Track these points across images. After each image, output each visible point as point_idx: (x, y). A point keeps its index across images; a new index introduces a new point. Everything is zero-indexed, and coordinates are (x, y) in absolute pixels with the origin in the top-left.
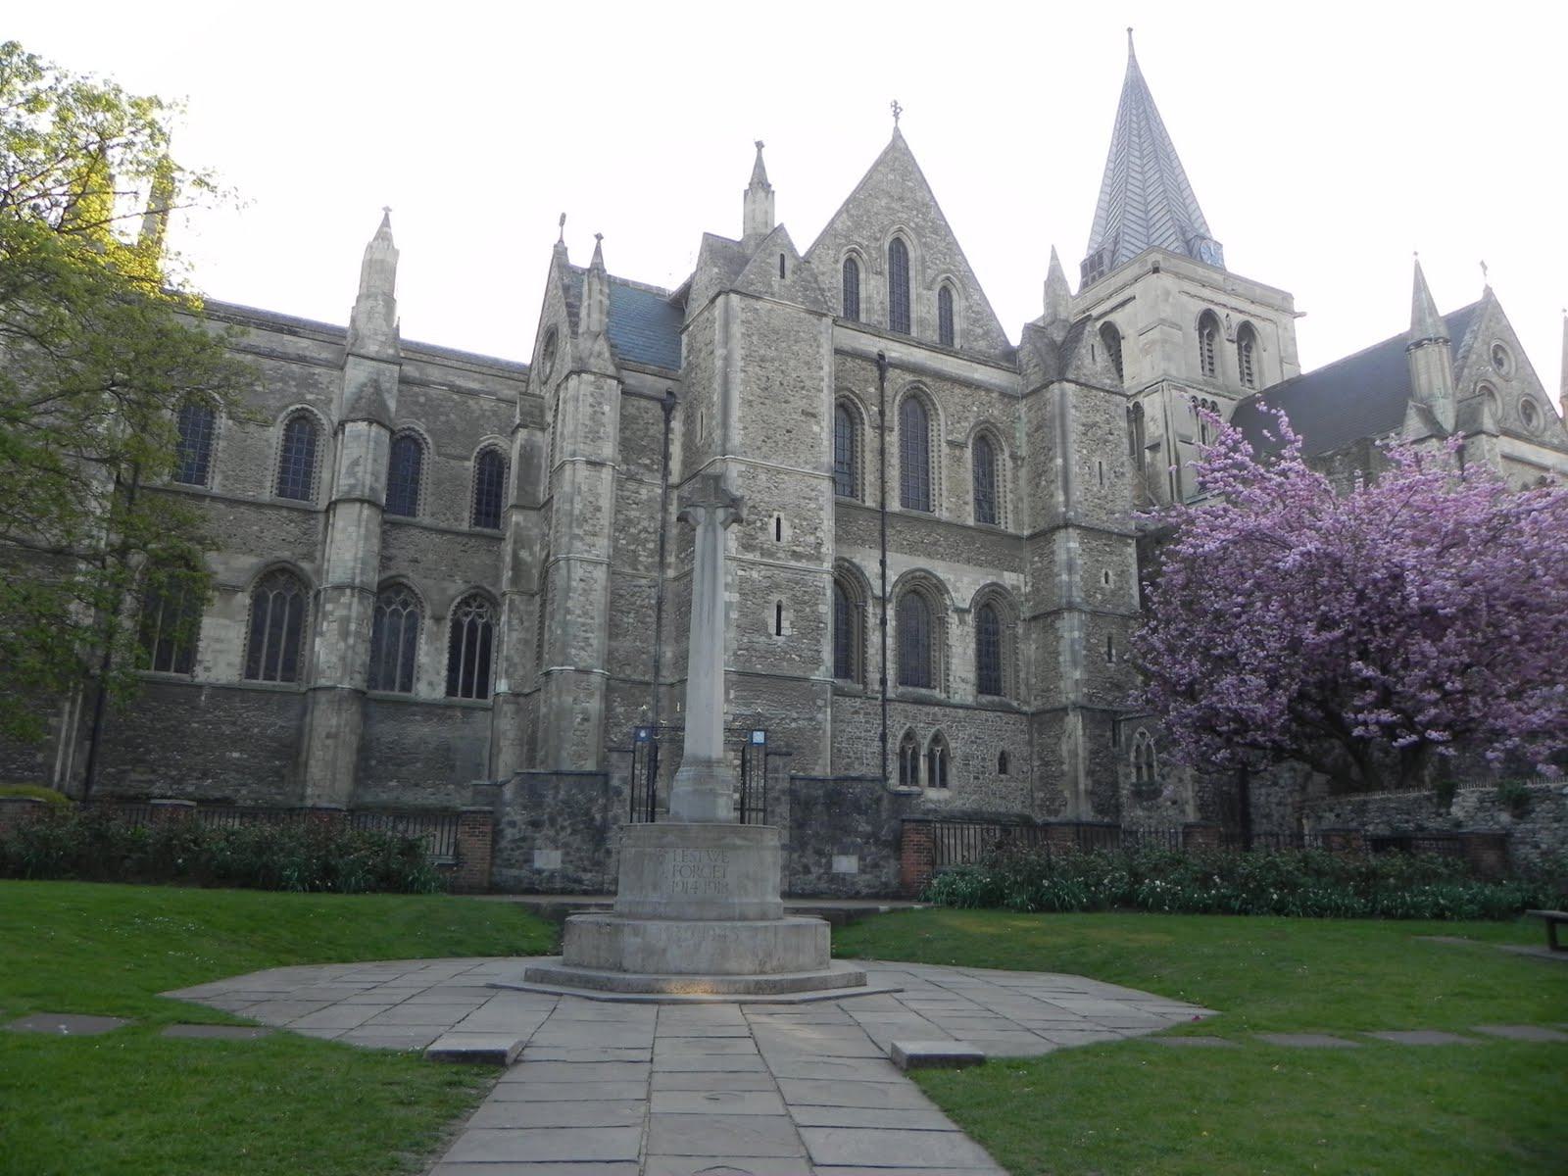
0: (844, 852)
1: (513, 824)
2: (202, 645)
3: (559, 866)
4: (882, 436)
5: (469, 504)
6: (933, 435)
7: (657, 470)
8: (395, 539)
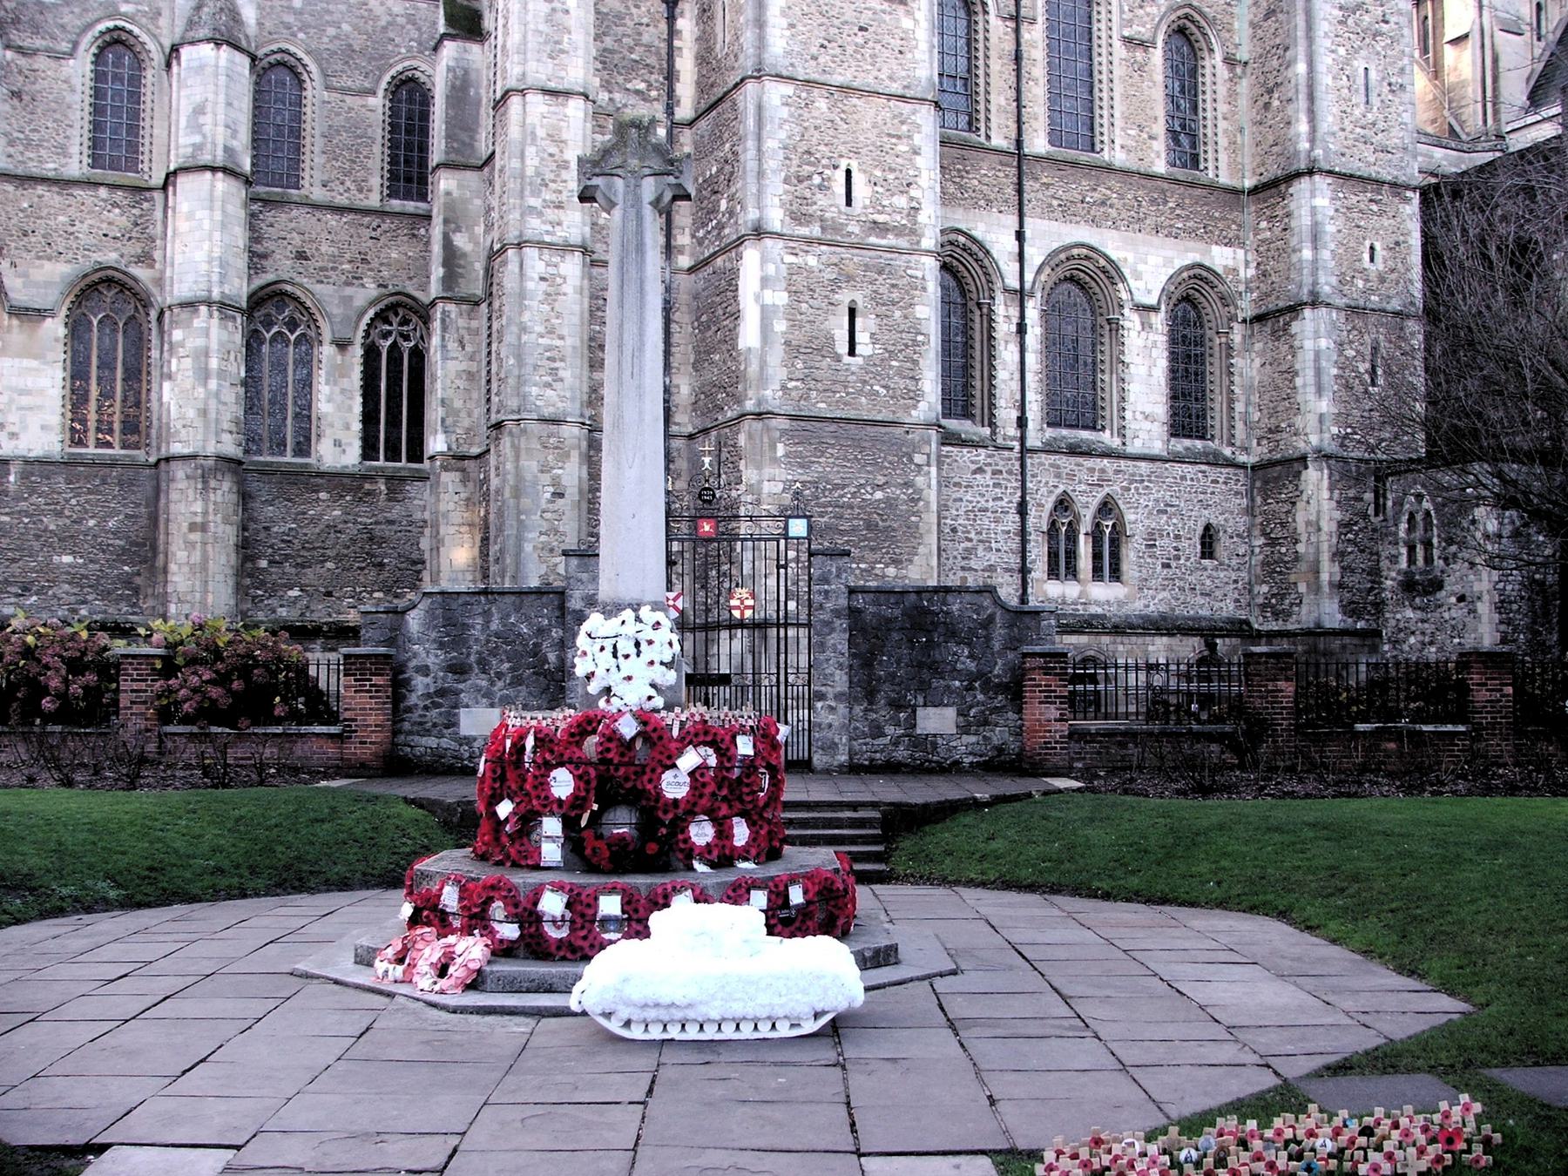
1: (424, 670)
4: (1017, 31)
5: (378, 164)
6: (1099, 28)
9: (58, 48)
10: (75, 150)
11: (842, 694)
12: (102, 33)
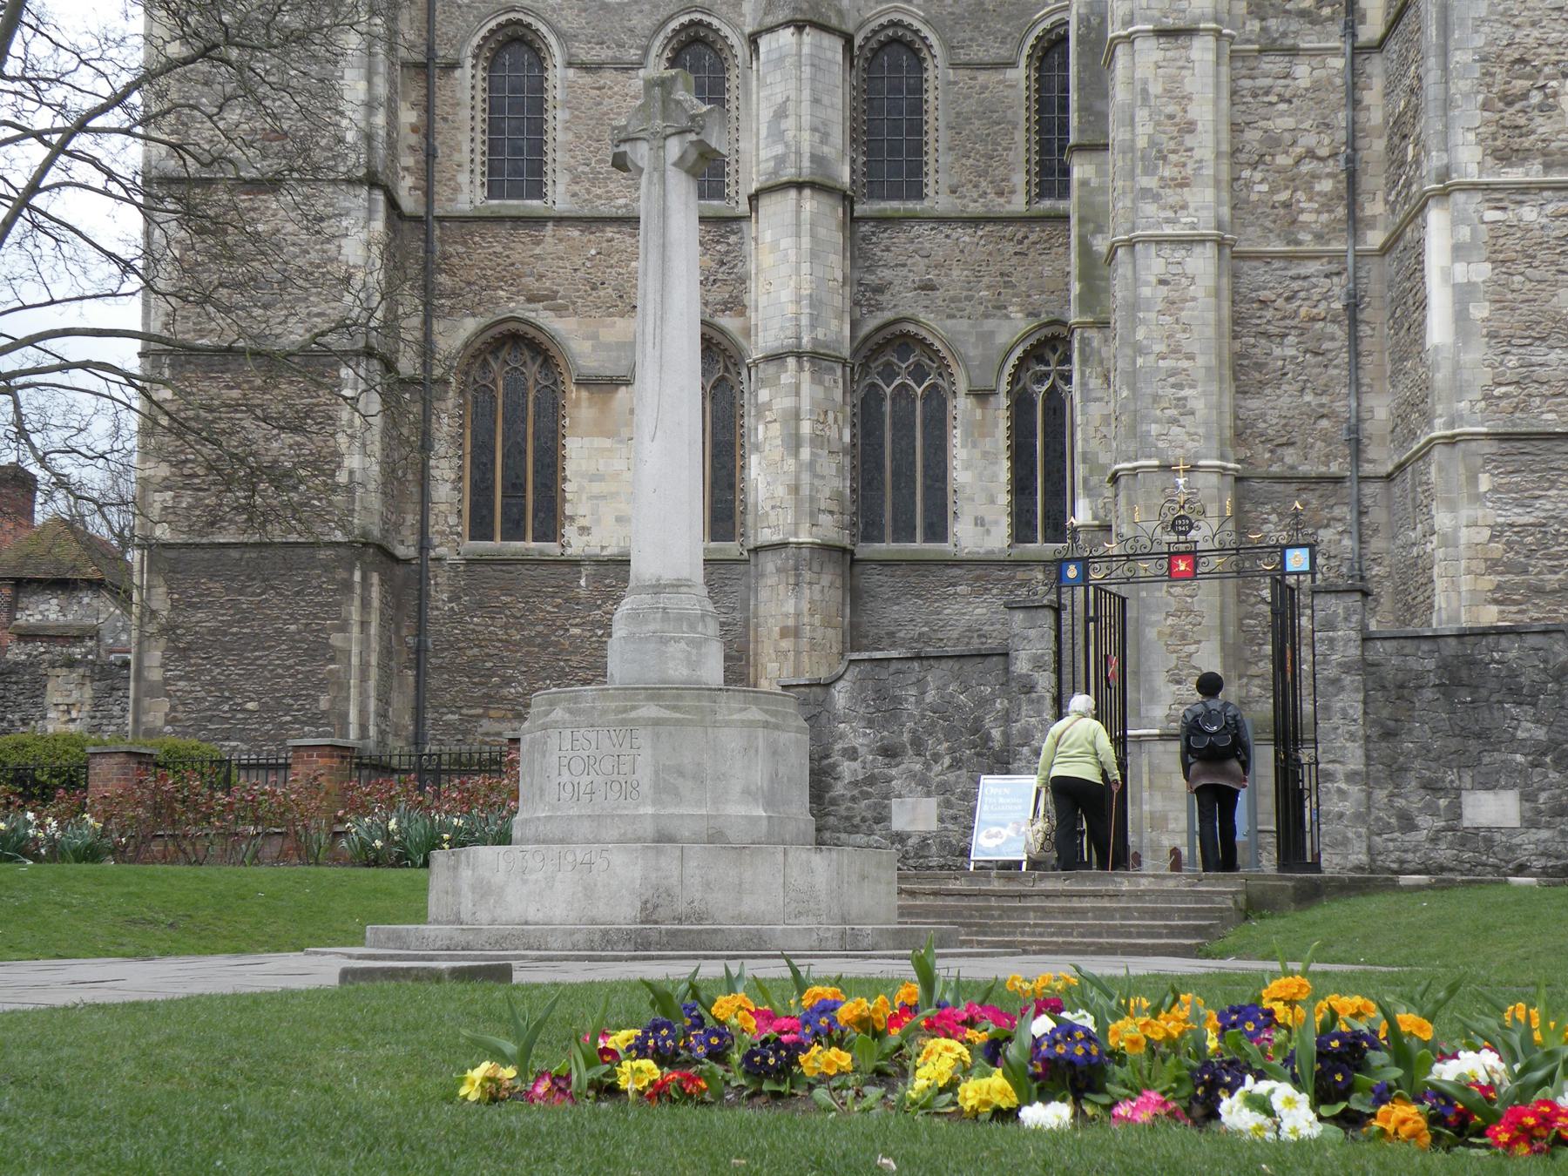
0: (1489, 785)
1: (852, 754)
2: (568, 487)
3: (934, 826)
5: (1023, 157)
7: (1331, 19)
8: (888, 249)
9: (626, 58)
11: (1356, 773)
12: (676, 32)
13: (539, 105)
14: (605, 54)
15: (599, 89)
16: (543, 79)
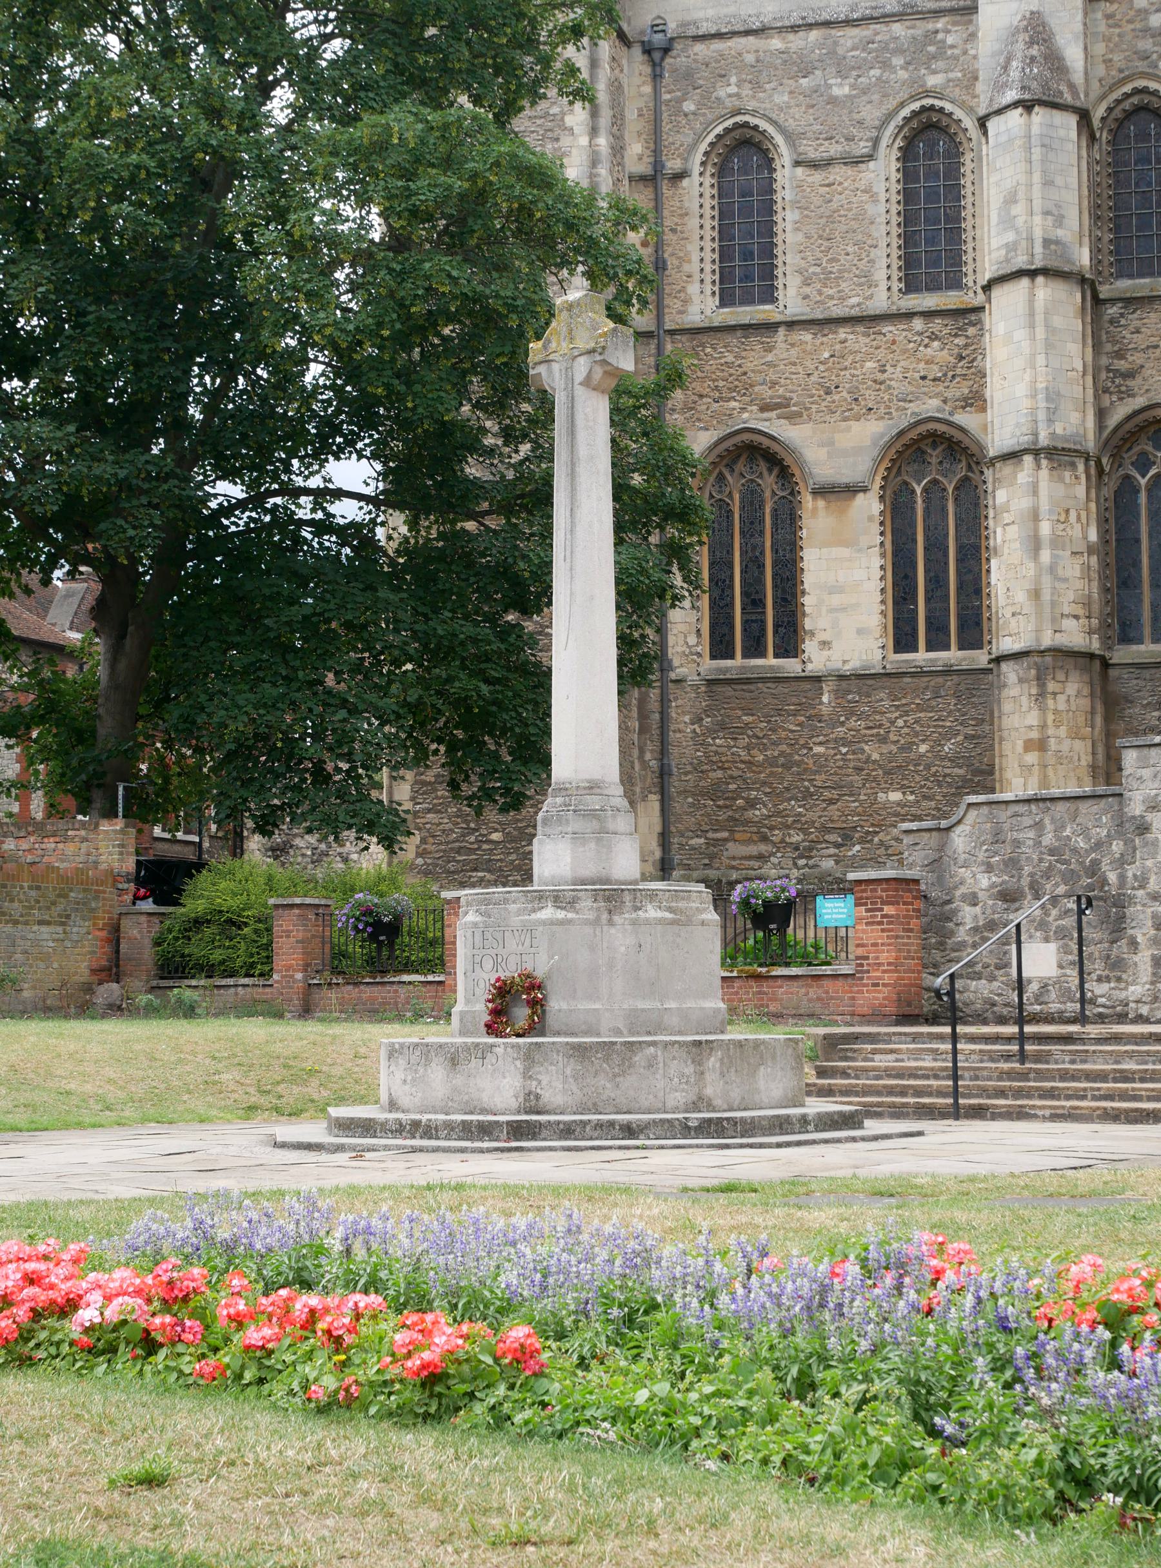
2: (807, 600)
10: (880, 275)
13: (768, 208)
14: (834, 149)
15: (828, 185)
16: (772, 180)
